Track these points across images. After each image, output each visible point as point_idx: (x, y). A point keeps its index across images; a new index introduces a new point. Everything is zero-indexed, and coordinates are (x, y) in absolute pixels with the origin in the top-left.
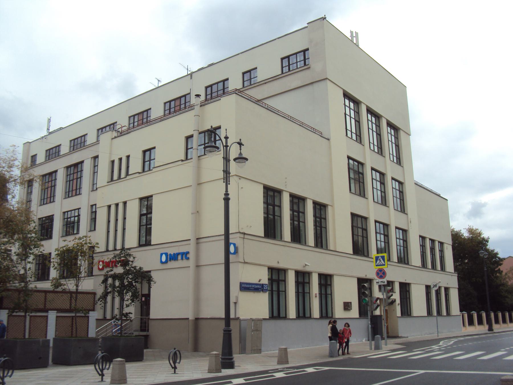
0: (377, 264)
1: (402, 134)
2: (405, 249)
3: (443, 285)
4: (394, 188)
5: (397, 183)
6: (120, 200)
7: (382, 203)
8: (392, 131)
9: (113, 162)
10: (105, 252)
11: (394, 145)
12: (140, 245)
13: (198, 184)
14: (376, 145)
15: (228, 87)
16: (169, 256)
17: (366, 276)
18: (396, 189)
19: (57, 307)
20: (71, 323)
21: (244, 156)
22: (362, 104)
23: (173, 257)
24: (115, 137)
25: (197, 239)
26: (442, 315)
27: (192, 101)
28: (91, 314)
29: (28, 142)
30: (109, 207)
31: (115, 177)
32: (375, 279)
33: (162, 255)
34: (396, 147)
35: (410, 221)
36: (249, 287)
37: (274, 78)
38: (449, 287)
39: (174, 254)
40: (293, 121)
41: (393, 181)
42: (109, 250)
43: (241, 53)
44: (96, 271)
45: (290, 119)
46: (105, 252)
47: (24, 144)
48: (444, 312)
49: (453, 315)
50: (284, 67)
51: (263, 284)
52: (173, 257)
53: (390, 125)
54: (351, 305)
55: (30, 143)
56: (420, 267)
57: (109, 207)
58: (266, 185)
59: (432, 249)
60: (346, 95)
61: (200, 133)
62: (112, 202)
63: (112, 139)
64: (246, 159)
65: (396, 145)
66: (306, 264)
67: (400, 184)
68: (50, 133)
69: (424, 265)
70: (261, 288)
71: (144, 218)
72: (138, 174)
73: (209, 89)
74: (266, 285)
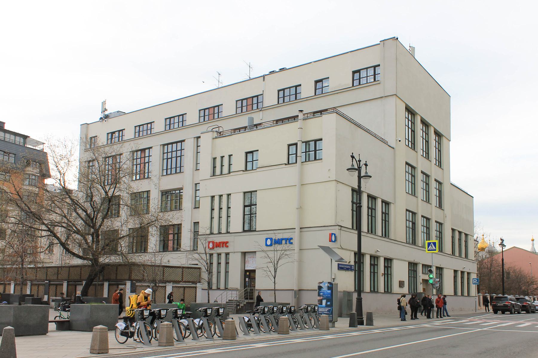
0: (429, 249)
1: (444, 140)
2: (440, 239)
3: (466, 270)
4: (407, 172)
5: (410, 168)
6: (225, 192)
7: (412, 194)
8: (410, 116)
9: (215, 159)
10: (209, 234)
11: (410, 130)
12: (244, 231)
13: (301, 185)
14: (410, 141)
15: (301, 93)
16: (273, 241)
17: (414, 260)
18: (409, 173)
19: (172, 279)
20: (183, 292)
21: (369, 174)
22: (432, 127)
23: (279, 242)
24: (216, 138)
25: (301, 228)
26: (464, 295)
27: (264, 100)
28: (198, 285)
29: (86, 124)
30: (213, 197)
31: (218, 171)
32: (420, 263)
33: (267, 240)
34: (412, 132)
35: (446, 216)
36: (343, 268)
37: (345, 90)
38: (470, 272)
39: (279, 239)
40: (370, 133)
41: (407, 166)
42: (222, 233)
43: (314, 62)
44: (201, 249)
45: (367, 131)
46: (209, 234)
47: (81, 125)
48: (466, 294)
49: (472, 296)
50: (355, 80)
51: (351, 265)
52: (279, 242)
53: (437, 134)
54: (404, 283)
55: (88, 124)
56: (451, 255)
57: (213, 197)
58: (353, 187)
59: (460, 239)
60: (408, 109)
61: (303, 142)
62: (216, 193)
63: (213, 139)
64: (370, 177)
65: (412, 131)
66: (377, 251)
67: (427, 177)
68: (107, 117)
69: (453, 253)
70: (350, 268)
71: (247, 209)
72: (242, 172)
73: (281, 93)
74: (353, 266)
